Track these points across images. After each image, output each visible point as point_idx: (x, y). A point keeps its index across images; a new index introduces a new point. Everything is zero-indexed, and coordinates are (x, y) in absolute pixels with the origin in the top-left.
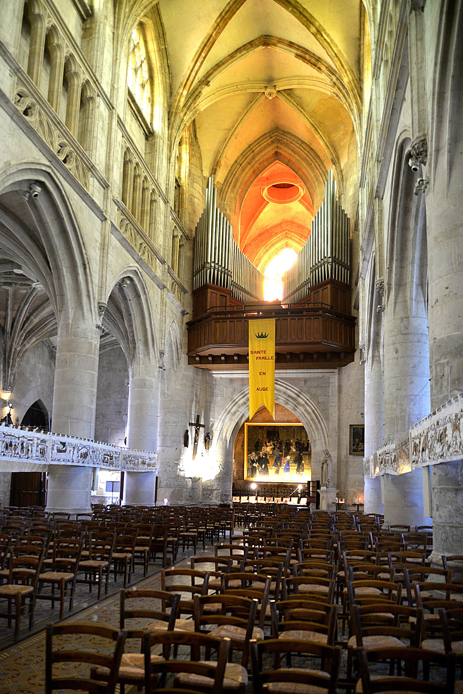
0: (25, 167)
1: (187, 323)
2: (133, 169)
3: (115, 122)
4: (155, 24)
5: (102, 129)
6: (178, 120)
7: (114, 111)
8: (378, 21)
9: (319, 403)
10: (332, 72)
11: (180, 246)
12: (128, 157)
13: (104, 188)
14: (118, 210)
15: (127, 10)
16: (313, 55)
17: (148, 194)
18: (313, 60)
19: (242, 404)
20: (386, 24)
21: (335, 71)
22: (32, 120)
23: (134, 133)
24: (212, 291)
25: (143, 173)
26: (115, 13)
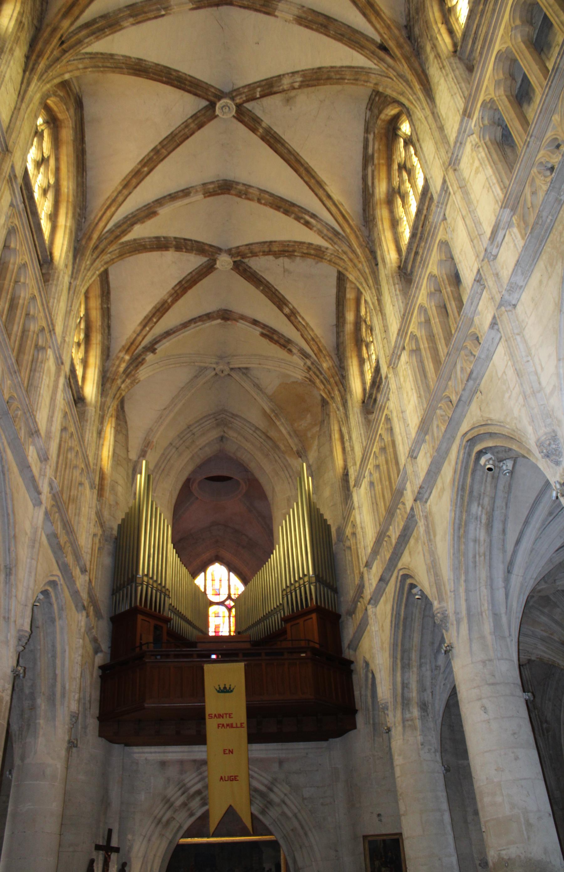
1: (101, 667)
5: (48, 386)
7: (63, 367)
9: (304, 799)
13: (41, 461)
16: (282, 336)
18: (282, 341)
19: (180, 806)
24: (144, 618)
26: (74, 264)
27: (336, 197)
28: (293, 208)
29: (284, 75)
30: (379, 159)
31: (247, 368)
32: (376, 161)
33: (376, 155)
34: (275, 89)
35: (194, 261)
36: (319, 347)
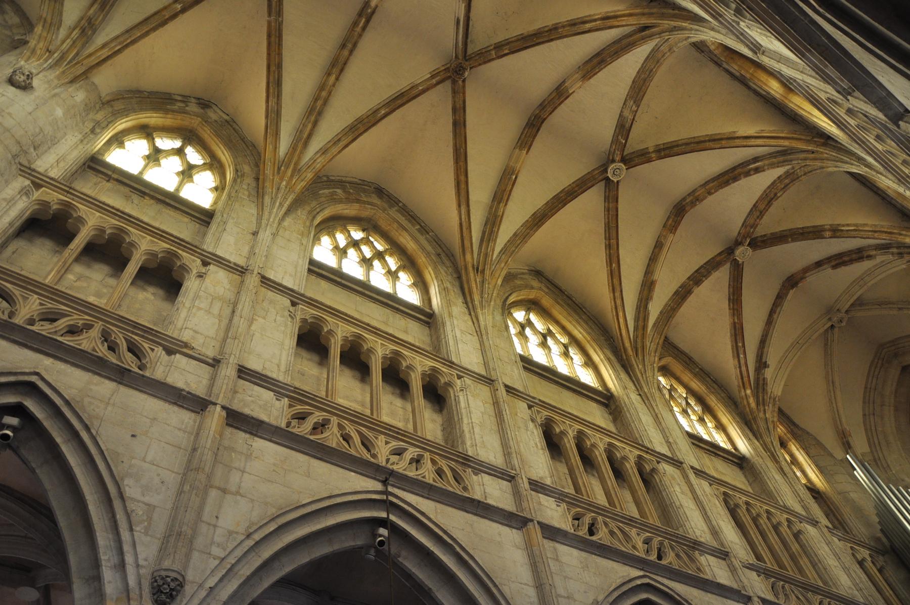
0: (616, 594)
2: (746, 513)
3: (692, 476)
4: (676, 357)
5: (682, 493)
6: (762, 425)
7: (684, 465)
8: (881, 169)
10: (884, 248)
11: (880, 571)
12: (732, 503)
13: (725, 559)
14: (759, 576)
15: (640, 367)
16: (850, 252)
17: (784, 529)
20: (891, 161)
21: (887, 244)
22: (603, 535)
23: (724, 471)
25: (760, 508)
27: (751, 132)
28: (736, 172)
29: (622, 111)
30: (747, 72)
31: (858, 299)
32: (748, 76)
33: (743, 72)
34: (627, 125)
35: (722, 275)
36: (886, 232)
